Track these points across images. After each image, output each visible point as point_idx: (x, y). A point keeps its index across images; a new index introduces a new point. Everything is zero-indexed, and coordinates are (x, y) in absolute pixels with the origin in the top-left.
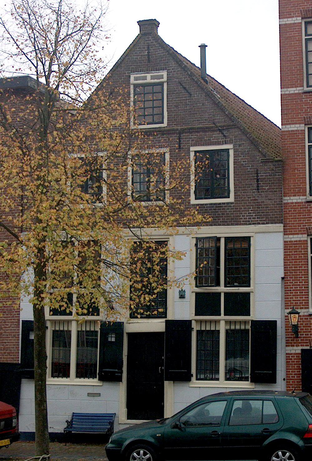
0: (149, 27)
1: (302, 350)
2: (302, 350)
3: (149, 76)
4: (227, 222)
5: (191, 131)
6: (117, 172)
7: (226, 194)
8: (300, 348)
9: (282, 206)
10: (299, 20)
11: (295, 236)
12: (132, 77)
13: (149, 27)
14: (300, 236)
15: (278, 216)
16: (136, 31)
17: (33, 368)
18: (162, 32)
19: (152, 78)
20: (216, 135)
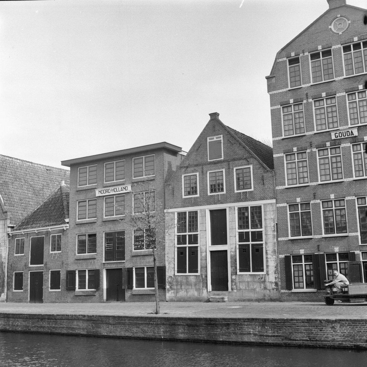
0: (214, 116)
1: (285, 256)
2: (285, 256)
3: (215, 137)
4: (251, 200)
5: (234, 160)
6: (37, 278)
7: (252, 228)
8: (284, 255)
9: (274, 190)
10: (279, 106)
11: (281, 204)
12: (208, 138)
13: (214, 116)
14: (283, 204)
15: (358, 324)
16: (209, 118)
17: (197, 231)
18: (221, 118)
19: (217, 138)
20: (244, 161)
